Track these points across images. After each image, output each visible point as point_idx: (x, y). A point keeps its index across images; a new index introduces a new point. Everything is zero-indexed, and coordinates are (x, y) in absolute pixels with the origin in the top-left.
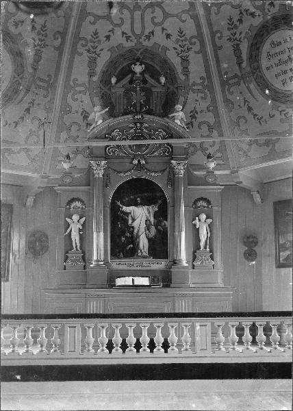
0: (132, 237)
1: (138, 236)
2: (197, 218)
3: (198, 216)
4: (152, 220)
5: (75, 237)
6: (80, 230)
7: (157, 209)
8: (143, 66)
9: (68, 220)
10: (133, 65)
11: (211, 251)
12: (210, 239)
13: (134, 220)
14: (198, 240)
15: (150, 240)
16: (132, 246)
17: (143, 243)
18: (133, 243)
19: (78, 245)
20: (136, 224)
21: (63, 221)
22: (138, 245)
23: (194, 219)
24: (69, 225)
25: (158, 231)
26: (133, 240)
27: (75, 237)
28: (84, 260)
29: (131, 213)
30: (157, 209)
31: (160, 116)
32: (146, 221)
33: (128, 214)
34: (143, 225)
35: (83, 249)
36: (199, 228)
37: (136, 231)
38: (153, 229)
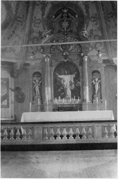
1: (66, 89)
2: (94, 80)
4: (73, 81)
7: (75, 76)
11: (101, 95)
12: (100, 89)
15: (72, 90)
16: (63, 93)
17: (69, 93)
20: (65, 83)
26: (64, 91)
27: (37, 89)
29: (62, 78)
30: (75, 76)
33: (61, 79)
34: (69, 84)
37: (65, 86)
38: (73, 86)
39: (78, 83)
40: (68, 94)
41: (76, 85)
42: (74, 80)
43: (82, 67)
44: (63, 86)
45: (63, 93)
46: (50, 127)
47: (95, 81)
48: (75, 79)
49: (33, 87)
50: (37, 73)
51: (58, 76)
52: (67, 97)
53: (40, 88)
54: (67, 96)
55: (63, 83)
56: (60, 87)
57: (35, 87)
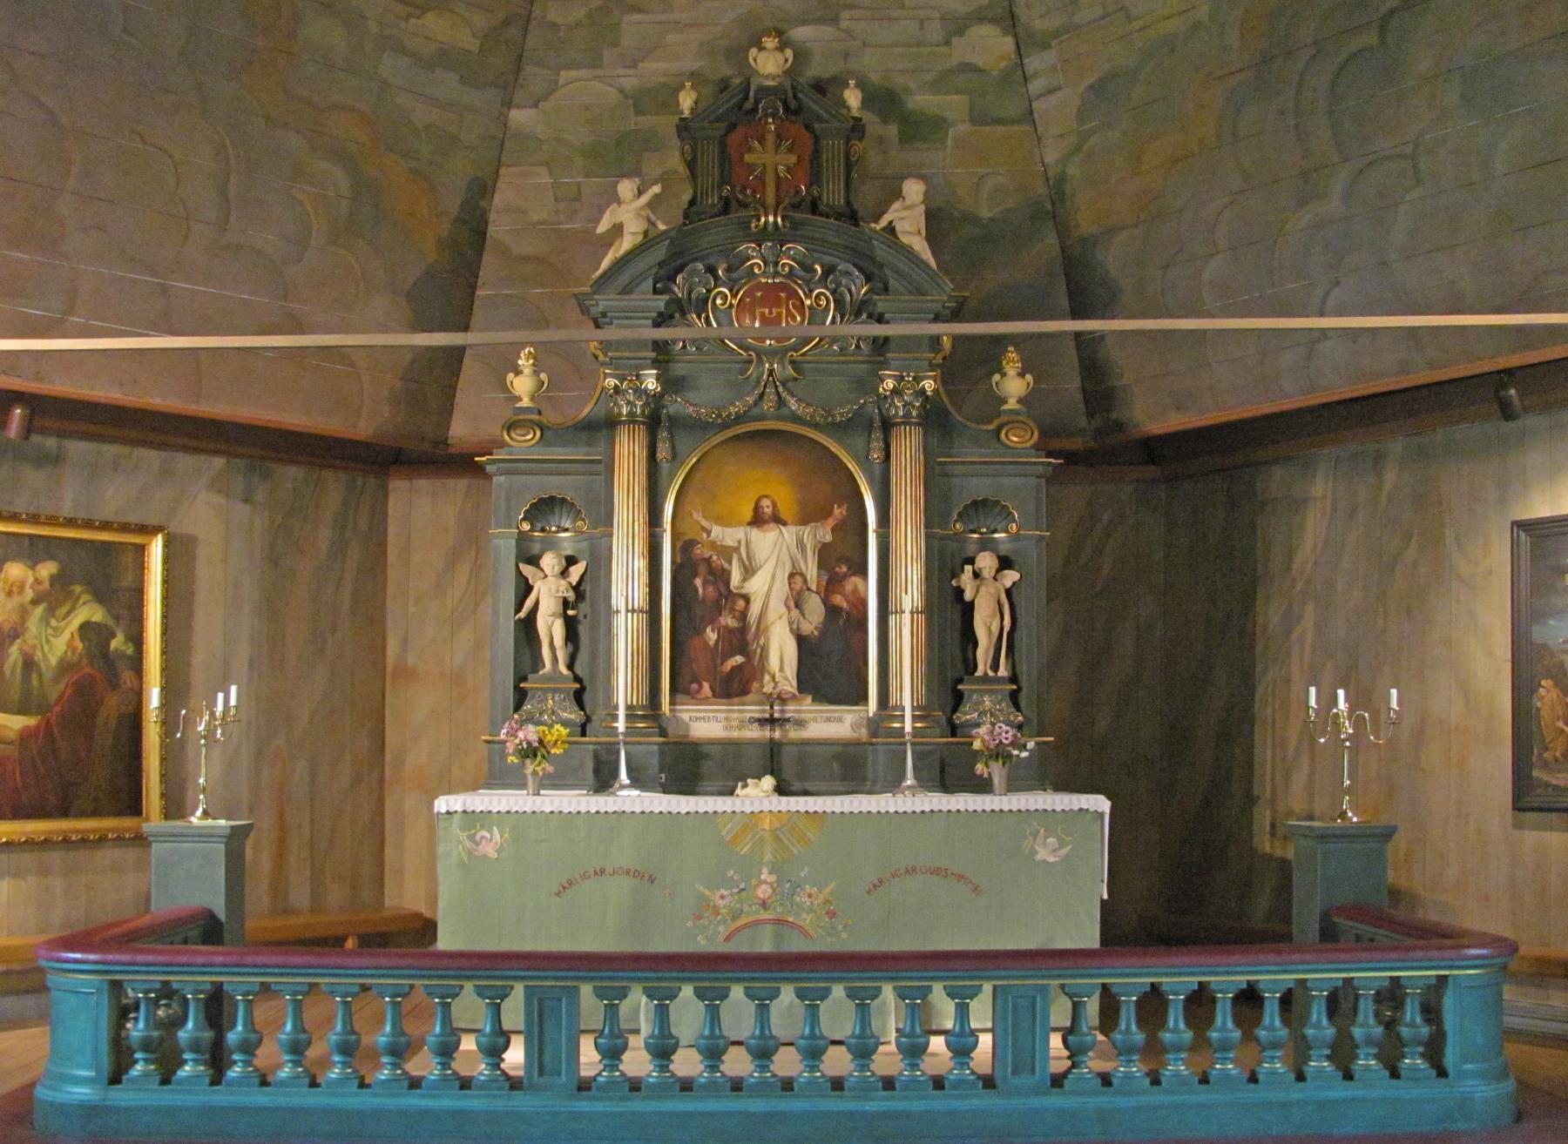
0: (743, 629)
1: (762, 629)
2: (968, 568)
3: (971, 561)
4: (811, 571)
5: (550, 627)
6: (566, 603)
7: (829, 538)
8: (789, 53)
9: (527, 570)
10: (753, 51)
13: (749, 571)
14: (969, 639)
15: (801, 640)
16: (739, 659)
18: (743, 649)
19: (561, 655)
20: (756, 586)
21: (513, 575)
22: (765, 650)
23: (956, 573)
24: (528, 589)
25: (832, 611)
26: (742, 639)
27: (550, 627)
28: (579, 697)
29: (737, 549)
30: (829, 538)
31: (1081, 359)
32: (791, 576)
33: (727, 552)
34: (781, 588)
35: (852, 198)
36: (972, 603)
37: (755, 609)
38: (815, 610)
39: (849, 587)
40: (774, 663)
41: (838, 600)
42: (821, 565)
43: (53, 1032)
44: (741, 603)
45: (739, 659)
46: (1060, 88)
47: (976, 575)
48: (825, 556)
49: (518, 610)
50: (43, 519)
51: (709, 533)
52: (768, 688)
53: (570, 612)
54: (767, 678)
55: (744, 580)
56: (718, 610)
57: (537, 603)
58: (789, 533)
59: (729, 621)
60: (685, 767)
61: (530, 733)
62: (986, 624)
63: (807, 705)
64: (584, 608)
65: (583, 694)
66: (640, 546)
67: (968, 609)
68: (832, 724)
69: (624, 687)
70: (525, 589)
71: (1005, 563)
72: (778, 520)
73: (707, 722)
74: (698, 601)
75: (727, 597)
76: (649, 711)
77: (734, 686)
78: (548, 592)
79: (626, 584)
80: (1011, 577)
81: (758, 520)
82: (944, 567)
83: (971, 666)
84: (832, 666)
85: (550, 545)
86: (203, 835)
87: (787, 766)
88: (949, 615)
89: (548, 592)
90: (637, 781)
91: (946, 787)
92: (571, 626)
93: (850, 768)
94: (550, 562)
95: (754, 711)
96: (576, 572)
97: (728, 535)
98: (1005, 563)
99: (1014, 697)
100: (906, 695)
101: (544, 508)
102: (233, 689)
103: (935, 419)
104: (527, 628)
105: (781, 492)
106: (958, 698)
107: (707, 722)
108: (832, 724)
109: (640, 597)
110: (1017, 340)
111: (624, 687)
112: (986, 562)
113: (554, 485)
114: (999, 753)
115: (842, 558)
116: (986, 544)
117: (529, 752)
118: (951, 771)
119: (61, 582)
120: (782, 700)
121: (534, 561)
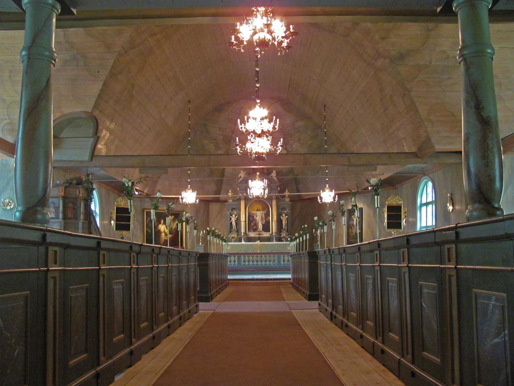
4: (264, 216)
5: (234, 224)
13: (256, 216)
15: (263, 225)
20: (257, 218)
25: (266, 221)
26: (256, 225)
27: (234, 224)
28: (237, 232)
34: (260, 218)
58: (261, 212)
59: (254, 222)
60: (249, 239)
61: (233, 236)
62: (284, 223)
63: (263, 232)
64: (238, 221)
65: (238, 231)
66: (244, 214)
67: (282, 221)
68: (266, 235)
69: (243, 231)
70: (231, 219)
71: (286, 215)
72: (260, 210)
73: (252, 234)
74: (251, 219)
75: (254, 220)
76: (245, 233)
77: (255, 230)
78: (233, 219)
79: (243, 218)
80: (287, 217)
81: (257, 210)
82: (279, 215)
83: (282, 227)
84: (266, 227)
85: (234, 213)
86: (201, 246)
87: (261, 239)
88: (279, 222)
89: (233, 219)
90: (276, 241)
91: (279, 241)
92: (236, 223)
93: (269, 239)
94: (234, 216)
95: (257, 233)
96: (237, 217)
97: (254, 212)
98: (286, 215)
99: (287, 231)
100: (274, 230)
101: (233, 209)
102: (308, 235)
103: (277, 198)
104: (231, 224)
105: (260, 207)
106: (281, 231)
107: (252, 234)
108: (266, 235)
109: (244, 219)
110: (494, 295)
111: (243, 231)
112: (284, 215)
113: (234, 207)
114: (284, 237)
115: (267, 215)
116: (284, 213)
117: (233, 238)
118: (279, 239)
119: (174, 218)
120: (261, 232)
121: (232, 215)
